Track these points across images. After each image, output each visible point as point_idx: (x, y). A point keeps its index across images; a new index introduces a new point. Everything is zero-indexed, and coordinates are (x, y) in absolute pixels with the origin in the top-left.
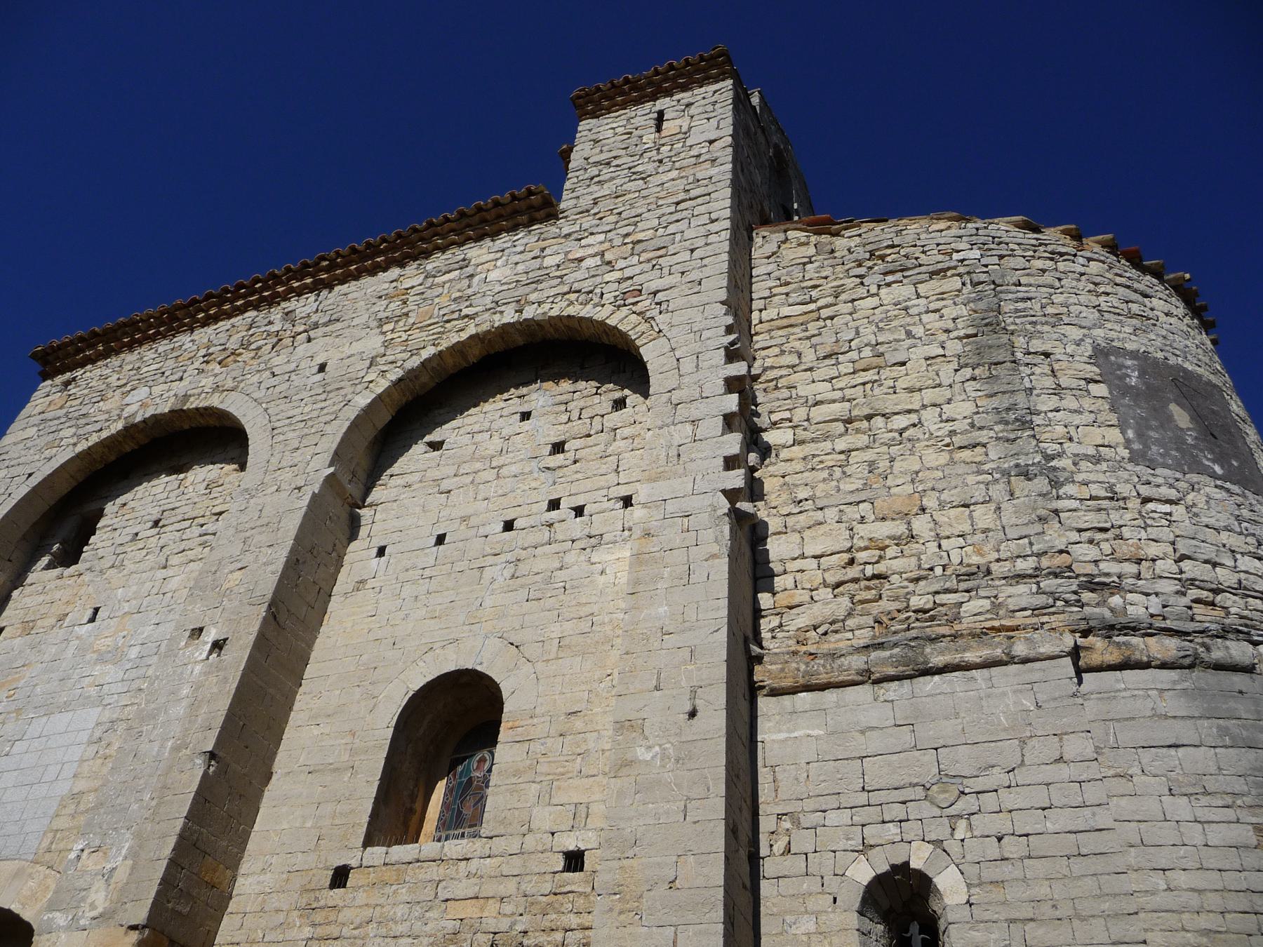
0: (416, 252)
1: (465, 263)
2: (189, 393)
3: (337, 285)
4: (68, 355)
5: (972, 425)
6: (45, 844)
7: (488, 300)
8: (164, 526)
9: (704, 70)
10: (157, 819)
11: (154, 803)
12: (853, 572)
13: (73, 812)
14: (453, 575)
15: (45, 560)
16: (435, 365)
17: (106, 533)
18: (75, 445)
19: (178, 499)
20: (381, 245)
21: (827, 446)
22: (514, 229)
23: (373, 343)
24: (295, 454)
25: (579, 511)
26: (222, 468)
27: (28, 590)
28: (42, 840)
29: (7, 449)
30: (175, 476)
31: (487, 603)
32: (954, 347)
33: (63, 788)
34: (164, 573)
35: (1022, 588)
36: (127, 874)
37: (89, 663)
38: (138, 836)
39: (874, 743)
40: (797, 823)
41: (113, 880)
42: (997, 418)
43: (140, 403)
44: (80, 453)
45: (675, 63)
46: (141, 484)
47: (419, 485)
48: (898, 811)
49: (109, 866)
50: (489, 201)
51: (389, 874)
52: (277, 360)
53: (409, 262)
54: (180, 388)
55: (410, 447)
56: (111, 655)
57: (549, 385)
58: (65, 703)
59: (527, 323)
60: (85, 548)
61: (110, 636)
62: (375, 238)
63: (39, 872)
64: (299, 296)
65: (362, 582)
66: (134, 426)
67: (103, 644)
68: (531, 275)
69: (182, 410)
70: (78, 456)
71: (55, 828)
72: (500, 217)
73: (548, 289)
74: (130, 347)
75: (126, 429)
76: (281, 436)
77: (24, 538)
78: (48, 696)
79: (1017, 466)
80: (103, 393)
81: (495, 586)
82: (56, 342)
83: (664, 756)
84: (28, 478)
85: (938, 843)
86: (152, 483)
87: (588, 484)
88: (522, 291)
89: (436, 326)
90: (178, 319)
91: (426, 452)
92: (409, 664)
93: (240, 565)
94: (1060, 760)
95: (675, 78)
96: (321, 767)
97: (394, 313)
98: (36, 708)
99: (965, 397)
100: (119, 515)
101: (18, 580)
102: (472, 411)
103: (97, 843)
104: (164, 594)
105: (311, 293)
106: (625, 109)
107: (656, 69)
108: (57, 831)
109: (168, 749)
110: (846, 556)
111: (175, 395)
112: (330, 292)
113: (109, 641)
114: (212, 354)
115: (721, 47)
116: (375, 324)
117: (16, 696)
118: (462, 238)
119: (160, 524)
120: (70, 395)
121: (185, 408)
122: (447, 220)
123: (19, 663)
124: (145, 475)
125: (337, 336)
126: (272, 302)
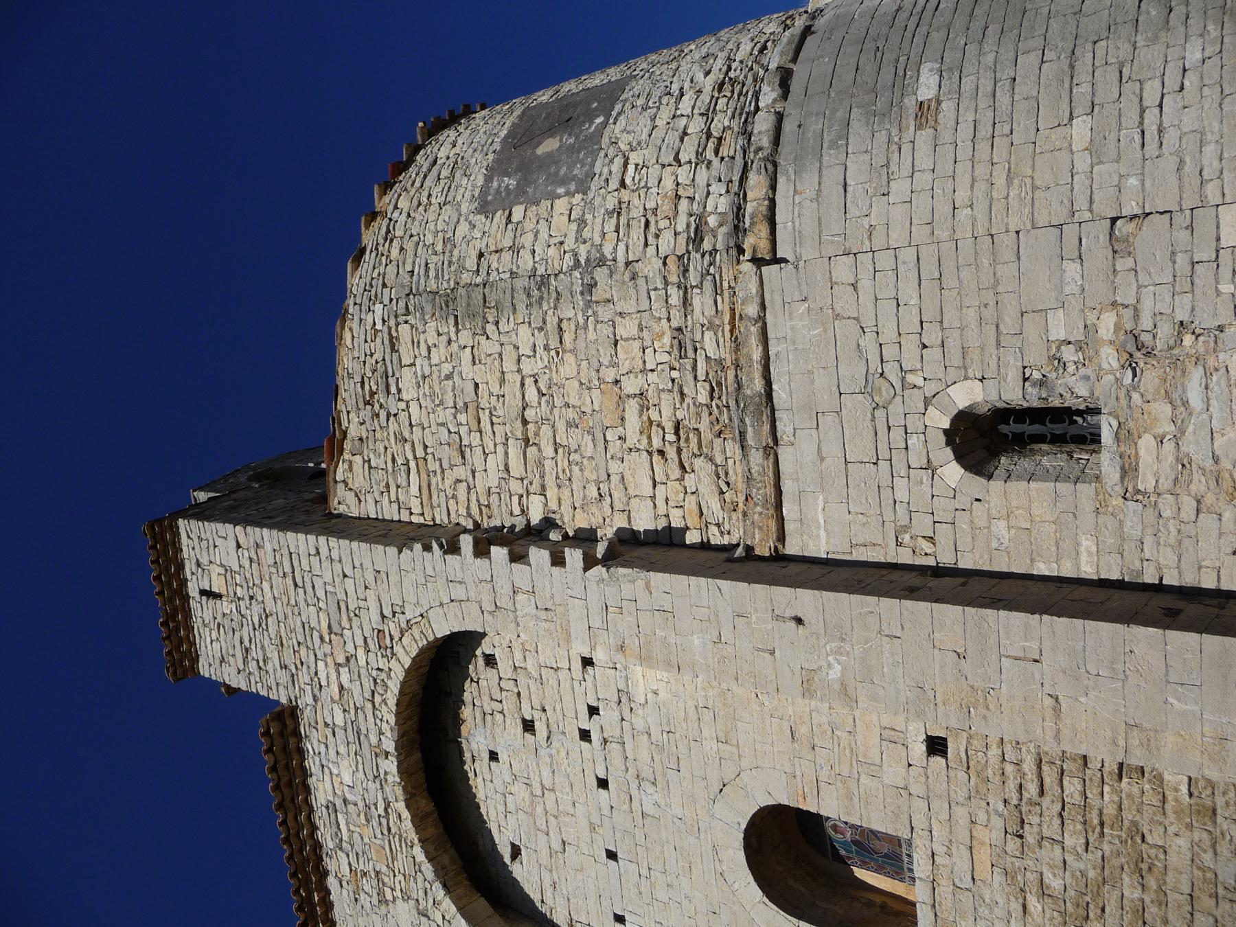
1: (331, 807)
9: (165, 546)
12: (671, 452)
20: (301, 895)
21: (548, 464)
22: (301, 753)
32: (465, 337)
39: (832, 449)
40: (905, 529)
42: (536, 307)
47: (554, 873)
48: (897, 434)
50: (270, 776)
53: (323, 866)
55: (515, 879)
68: (351, 740)
72: (287, 767)
73: (367, 723)
79: (582, 293)
85: (927, 402)
87: (567, 699)
88: (366, 750)
89: (392, 843)
91: (521, 863)
94: (854, 286)
95: (170, 576)
102: (483, 810)
106: (193, 627)
107: (157, 594)
110: (656, 457)
115: (145, 527)
116: (384, 909)
118: (304, 808)
122: (284, 822)
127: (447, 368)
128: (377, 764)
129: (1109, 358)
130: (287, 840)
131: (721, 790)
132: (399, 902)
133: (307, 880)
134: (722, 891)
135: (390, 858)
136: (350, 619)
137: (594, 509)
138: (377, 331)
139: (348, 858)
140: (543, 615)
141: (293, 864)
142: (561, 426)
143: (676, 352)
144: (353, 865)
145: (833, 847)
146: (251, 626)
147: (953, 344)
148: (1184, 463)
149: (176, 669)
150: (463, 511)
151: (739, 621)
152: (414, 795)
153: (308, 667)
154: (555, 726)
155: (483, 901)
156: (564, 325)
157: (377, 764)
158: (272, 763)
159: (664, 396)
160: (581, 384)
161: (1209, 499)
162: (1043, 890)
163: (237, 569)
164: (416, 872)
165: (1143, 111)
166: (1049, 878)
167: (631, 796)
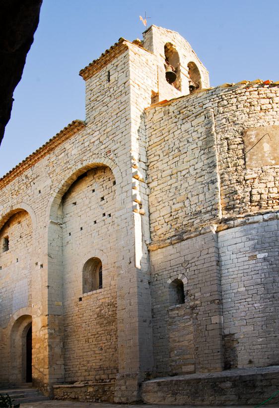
5: (202, 170)
7: (73, 162)
12: (171, 218)
21: (165, 184)
23: (49, 182)
25: (110, 215)
31: (94, 242)
32: (200, 143)
35: (208, 215)
39: (173, 257)
40: (158, 275)
42: (208, 166)
48: (176, 269)
51: (88, 297)
52: (29, 191)
54: (10, 204)
65: (68, 242)
67: (22, 266)
73: (88, 154)
79: (211, 180)
83: (126, 271)
85: (183, 274)
87: (110, 208)
88: (81, 157)
94: (208, 254)
99: (262, 106)
110: (170, 215)
116: (48, 175)
127: (190, 140)
129: (192, 304)
132: (50, 180)
136: (111, 139)
137: (156, 201)
138: (202, 107)
140: (123, 202)
142: (176, 185)
143: (196, 212)
146: (102, 99)
147: (195, 276)
148: (174, 318)
150: (151, 160)
151: (128, 251)
156: (203, 177)
159: (184, 213)
160: (187, 188)
161: (168, 322)
162: (101, 310)
163: (118, 86)
165: (245, 299)
166: (103, 311)
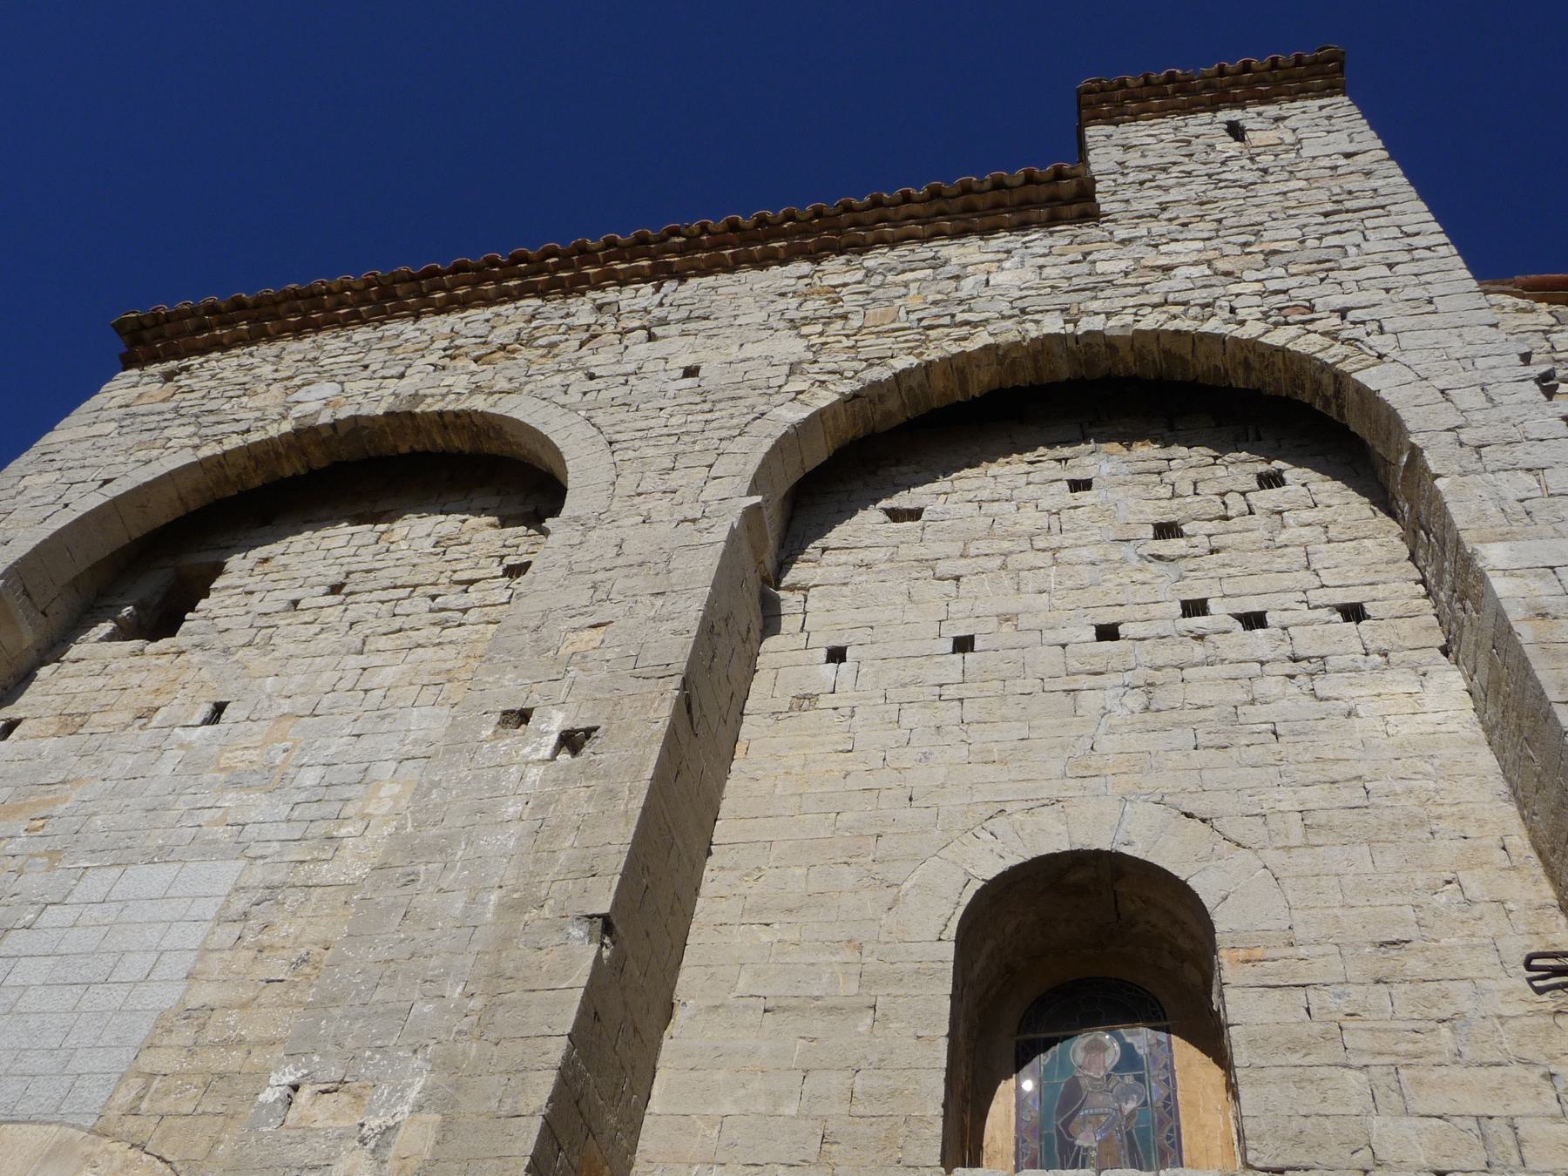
0: (844, 241)
1: (936, 264)
2: (421, 392)
3: (693, 276)
4: (179, 334)
6: (125, 1097)
8: (351, 593)
9: (1300, 78)
10: (493, 1036)
11: (475, 1004)
13: (190, 1042)
14: (1010, 700)
15: (106, 627)
16: (914, 384)
17: (230, 596)
18: (196, 447)
19: (378, 557)
20: (783, 223)
22: (1023, 226)
24: (667, 477)
26: (464, 521)
27: (69, 668)
28: (116, 1090)
29: (57, 447)
30: (370, 526)
33: (166, 996)
34: (362, 660)
36: (431, 1143)
37: (209, 786)
38: (447, 1064)
41: (391, 1153)
43: (324, 402)
44: (207, 459)
45: (1255, 62)
46: (299, 533)
47: (888, 565)
49: (374, 1123)
50: (988, 177)
53: (828, 256)
54: (406, 386)
55: (853, 513)
56: (258, 777)
57: (1115, 447)
58: (160, 848)
59: (1088, 340)
60: (189, 616)
61: (256, 748)
62: (775, 211)
63: (112, 1153)
64: (621, 286)
66: (314, 430)
68: (1075, 281)
69: (411, 415)
70: (201, 463)
71: (148, 1070)
72: (998, 206)
74: (298, 332)
75: (297, 433)
76: (630, 452)
77: (75, 583)
78: (123, 835)
80: (247, 387)
81: (1114, 720)
82: (164, 309)
84: (101, 486)
86: (322, 533)
89: (910, 332)
90: (394, 297)
91: (885, 522)
92: (956, 833)
93: (593, 621)
95: (1250, 85)
96: (794, 1002)
97: (817, 313)
98: (93, 852)
100: (255, 573)
101: (53, 649)
102: (966, 472)
103: (335, 1073)
104: (366, 691)
105: (646, 282)
106: (1163, 118)
107: (1222, 67)
108: (153, 1075)
109: (491, 907)
111: (393, 394)
112: (679, 285)
113: (252, 755)
114: (461, 347)
115: (1334, 47)
117: (45, 829)
118: (928, 229)
119: (346, 590)
120: (181, 387)
121: (418, 410)
122: (907, 198)
123: (55, 776)
124: (306, 522)
125: (710, 337)
126: (570, 289)
128: (1048, 311)
130: (877, 203)
131: (1189, 815)
133: (806, 233)
134: (966, 813)
135: (876, 330)
139: (855, 283)
141: (838, 211)
144: (844, 289)
145: (1050, 1043)
149: (1097, 93)
152: (1001, 363)
153: (43, 826)
154: (1192, 567)
155: (822, 457)
157: (1048, 311)
158: (1008, 182)
164: (866, 360)
167: (1101, 673)
